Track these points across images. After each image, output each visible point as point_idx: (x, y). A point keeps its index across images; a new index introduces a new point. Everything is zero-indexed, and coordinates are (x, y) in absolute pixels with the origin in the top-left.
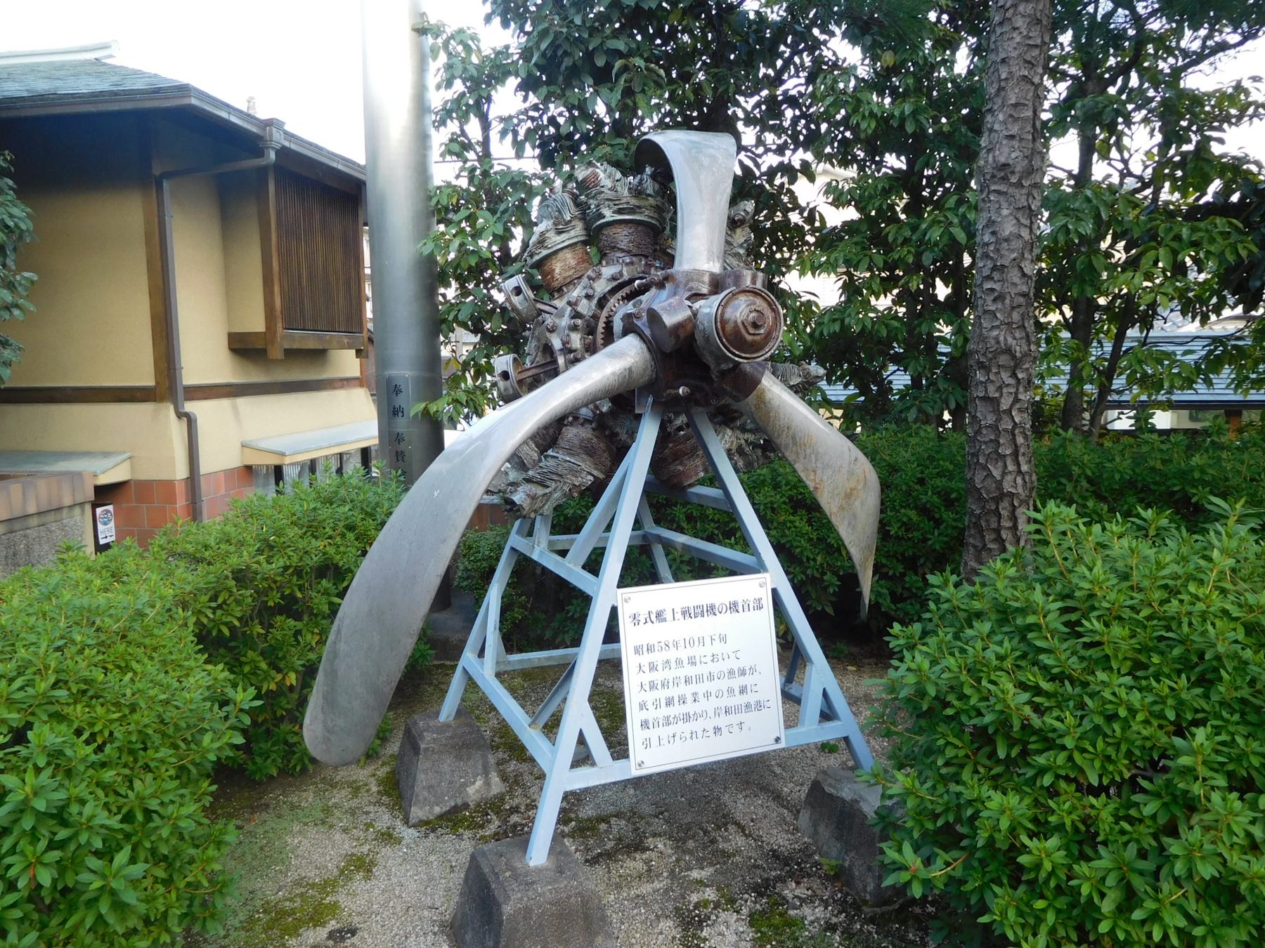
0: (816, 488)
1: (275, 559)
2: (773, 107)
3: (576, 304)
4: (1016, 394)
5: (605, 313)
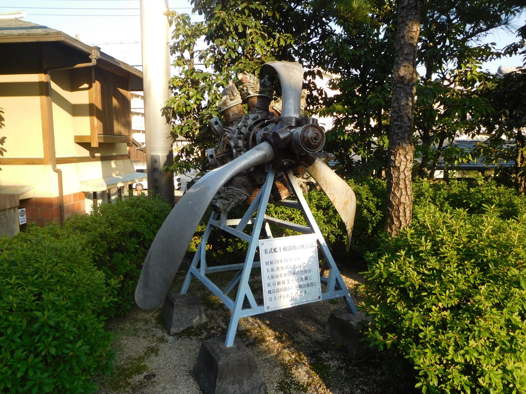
0: (334, 201)
1: (114, 229)
2: (307, 49)
3: (241, 129)
4: (406, 165)
5: (252, 133)
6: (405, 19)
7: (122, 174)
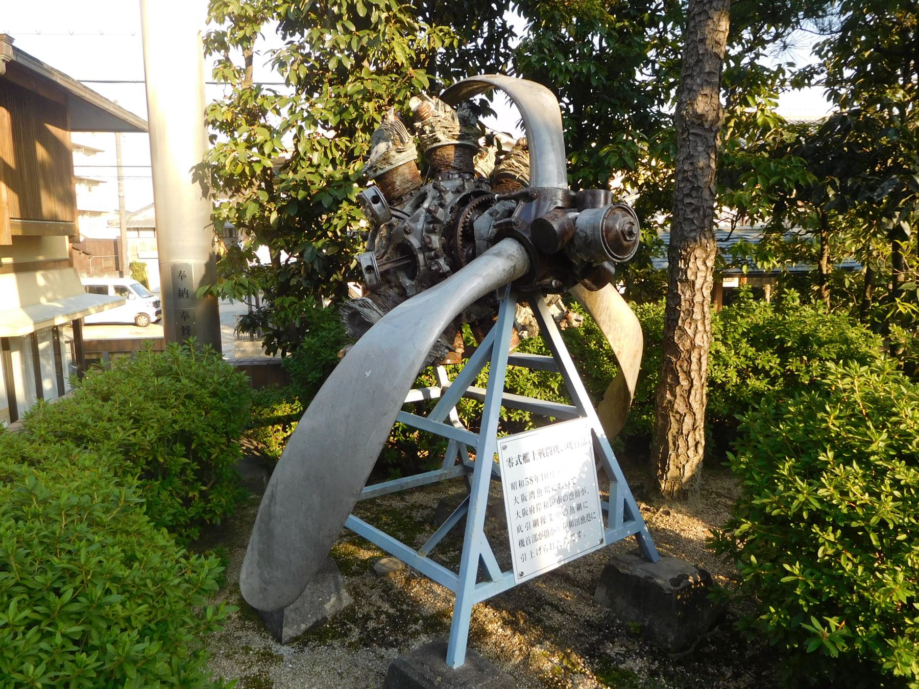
4: (705, 277)
6: (707, 7)
7: (59, 297)
